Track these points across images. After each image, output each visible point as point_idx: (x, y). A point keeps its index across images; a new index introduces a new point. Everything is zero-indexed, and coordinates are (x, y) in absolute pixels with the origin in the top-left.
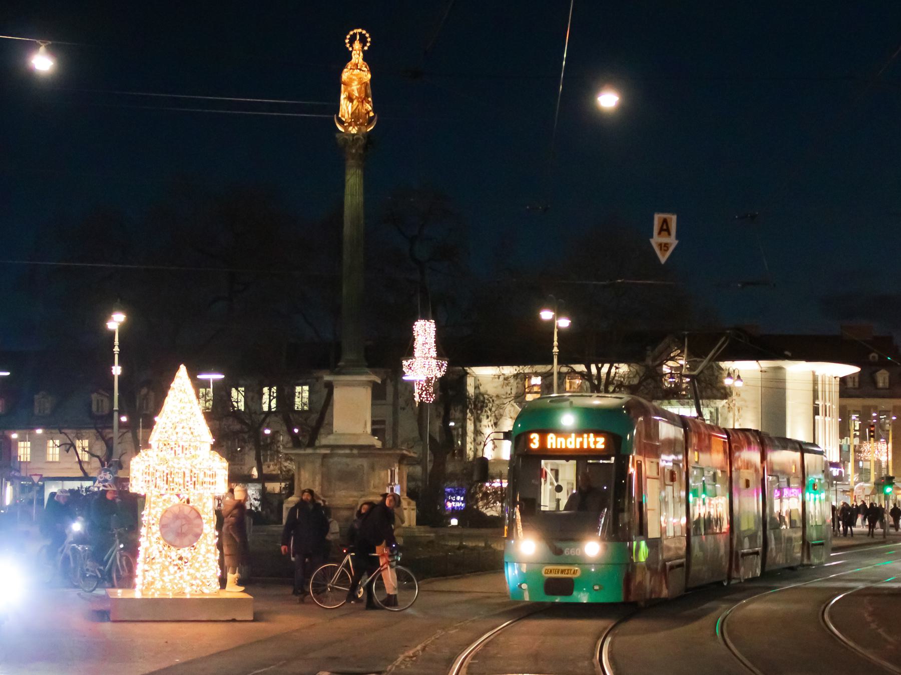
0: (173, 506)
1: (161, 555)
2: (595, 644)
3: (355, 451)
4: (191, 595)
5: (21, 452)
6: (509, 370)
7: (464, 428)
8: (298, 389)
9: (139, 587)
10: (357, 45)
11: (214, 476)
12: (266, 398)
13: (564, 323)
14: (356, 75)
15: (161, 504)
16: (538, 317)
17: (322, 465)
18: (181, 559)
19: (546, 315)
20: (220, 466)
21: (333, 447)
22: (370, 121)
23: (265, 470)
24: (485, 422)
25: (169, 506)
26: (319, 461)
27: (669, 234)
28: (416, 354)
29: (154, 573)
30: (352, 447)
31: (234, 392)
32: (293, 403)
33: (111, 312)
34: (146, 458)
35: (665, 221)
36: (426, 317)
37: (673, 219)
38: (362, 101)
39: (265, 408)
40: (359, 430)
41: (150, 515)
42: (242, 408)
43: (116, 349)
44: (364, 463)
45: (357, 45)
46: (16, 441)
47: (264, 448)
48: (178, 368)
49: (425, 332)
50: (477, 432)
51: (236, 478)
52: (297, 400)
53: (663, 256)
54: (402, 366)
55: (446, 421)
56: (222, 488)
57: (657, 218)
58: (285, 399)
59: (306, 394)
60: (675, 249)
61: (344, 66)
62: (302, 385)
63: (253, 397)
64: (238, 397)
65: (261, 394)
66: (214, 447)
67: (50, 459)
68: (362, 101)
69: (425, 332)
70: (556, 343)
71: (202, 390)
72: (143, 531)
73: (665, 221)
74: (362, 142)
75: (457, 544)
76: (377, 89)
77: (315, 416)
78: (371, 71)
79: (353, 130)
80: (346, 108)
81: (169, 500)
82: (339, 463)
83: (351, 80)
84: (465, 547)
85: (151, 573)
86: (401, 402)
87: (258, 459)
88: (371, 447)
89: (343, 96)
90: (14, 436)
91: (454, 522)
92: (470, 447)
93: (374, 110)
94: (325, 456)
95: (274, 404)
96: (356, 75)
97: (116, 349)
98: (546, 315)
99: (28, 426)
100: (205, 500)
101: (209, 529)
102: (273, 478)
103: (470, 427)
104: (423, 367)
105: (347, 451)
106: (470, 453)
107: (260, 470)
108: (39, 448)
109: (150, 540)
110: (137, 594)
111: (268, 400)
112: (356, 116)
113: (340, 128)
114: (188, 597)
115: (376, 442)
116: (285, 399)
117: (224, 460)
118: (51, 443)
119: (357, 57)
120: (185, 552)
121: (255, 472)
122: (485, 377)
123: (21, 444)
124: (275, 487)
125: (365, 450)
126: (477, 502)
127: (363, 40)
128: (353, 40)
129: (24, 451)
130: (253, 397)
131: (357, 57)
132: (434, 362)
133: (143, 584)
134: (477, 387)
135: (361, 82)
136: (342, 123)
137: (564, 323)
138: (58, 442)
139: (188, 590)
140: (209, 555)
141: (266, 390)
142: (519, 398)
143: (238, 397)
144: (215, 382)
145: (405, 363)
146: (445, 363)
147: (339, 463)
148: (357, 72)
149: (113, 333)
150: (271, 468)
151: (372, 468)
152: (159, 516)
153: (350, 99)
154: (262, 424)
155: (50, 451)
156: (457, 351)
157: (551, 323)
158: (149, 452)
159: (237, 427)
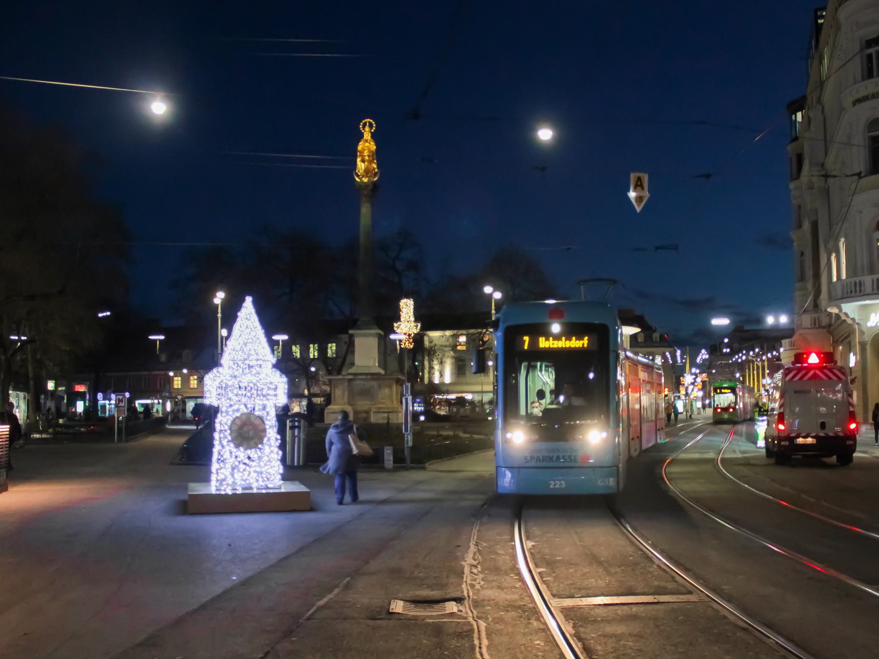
0: (242, 415)
1: (231, 456)
2: (628, 538)
3: (369, 377)
4: (258, 489)
5: (175, 382)
6: (448, 333)
7: (423, 365)
8: (330, 345)
9: (214, 483)
10: (367, 129)
11: (276, 389)
12: (311, 350)
13: (498, 295)
14: (367, 145)
15: (231, 413)
16: (482, 289)
17: (349, 385)
18: (249, 458)
19: (488, 290)
20: (281, 382)
21: (355, 374)
22: (376, 174)
23: (312, 391)
24: (435, 362)
25: (238, 414)
26: (346, 383)
27: (643, 189)
28: (402, 319)
29: (226, 472)
30: (366, 374)
31: (294, 348)
32: (327, 353)
33: (216, 291)
34: (218, 375)
35: (639, 179)
36: (408, 297)
37: (646, 178)
38: (370, 162)
39: (311, 356)
40: (371, 363)
41: (223, 422)
42: (299, 356)
43: (219, 315)
44: (374, 384)
45: (367, 129)
46: (173, 377)
47: (312, 379)
48: (244, 300)
49: (407, 306)
50: (431, 368)
51: (293, 394)
52: (329, 351)
53: (639, 206)
54: (393, 326)
55: (414, 362)
56: (283, 400)
57: (633, 176)
58: (323, 351)
59: (334, 348)
60: (648, 200)
61: (359, 141)
62: (332, 343)
63: (305, 350)
64: (296, 350)
65: (309, 348)
66: (275, 366)
67: (192, 386)
68: (370, 162)
69: (407, 306)
70: (493, 307)
71: (276, 347)
72: (216, 435)
73: (639, 179)
74: (370, 187)
75: (435, 433)
76: (379, 155)
77: (340, 361)
78: (376, 145)
79: (365, 180)
80: (361, 166)
81: (238, 410)
82: (359, 384)
83: (364, 150)
84: (441, 436)
85: (223, 471)
86: (389, 351)
87: (308, 384)
88: (379, 374)
89: (359, 160)
90: (171, 374)
91: (422, 418)
92: (426, 376)
93: (378, 168)
94: (350, 380)
95: (316, 354)
96: (367, 145)
97: (219, 315)
98: (488, 290)
99: (178, 369)
100: (268, 409)
101: (272, 434)
102: (317, 395)
103: (426, 363)
104: (406, 327)
105: (364, 377)
106: (426, 381)
107: (309, 391)
108: (186, 380)
109: (223, 446)
110: (213, 490)
111: (313, 352)
112: (367, 171)
113: (357, 179)
114: (255, 491)
115: (382, 372)
116: (323, 351)
117: (283, 376)
118: (192, 378)
119: (367, 136)
120: (252, 453)
121: (306, 392)
122: (435, 335)
123: (176, 378)
124: (318, 400)
125: (375, 376)
126: (435, 407)
127: (371, 126)
128: (365, 125)
129: (177, 383)
130: (305, 350)
131: (367, 136)
132: (413, 324)
133: (217, 480)
134: (431, 342)
135: (370, 151)
136: (358, 176)
137: (498, 295)
138: (196, 377)
139: (255, 485)
140: (272, 455)
141: (311, 346)
142: (454, 348)
143: (296, 350)
144: (283, 341)
145: (395, 325)
146: (419, 325)
147: (359, 384)
148: (367, 144)
149: (218, 305)
150: (315, 390)
151: (380, 387)
152: (229, 423)
153: (363, 161)
154: (310, 365)
155: (192, 382)
156: (427, 319)
157: (491, 295)
158: (220, 369)
159: (296, 366)
